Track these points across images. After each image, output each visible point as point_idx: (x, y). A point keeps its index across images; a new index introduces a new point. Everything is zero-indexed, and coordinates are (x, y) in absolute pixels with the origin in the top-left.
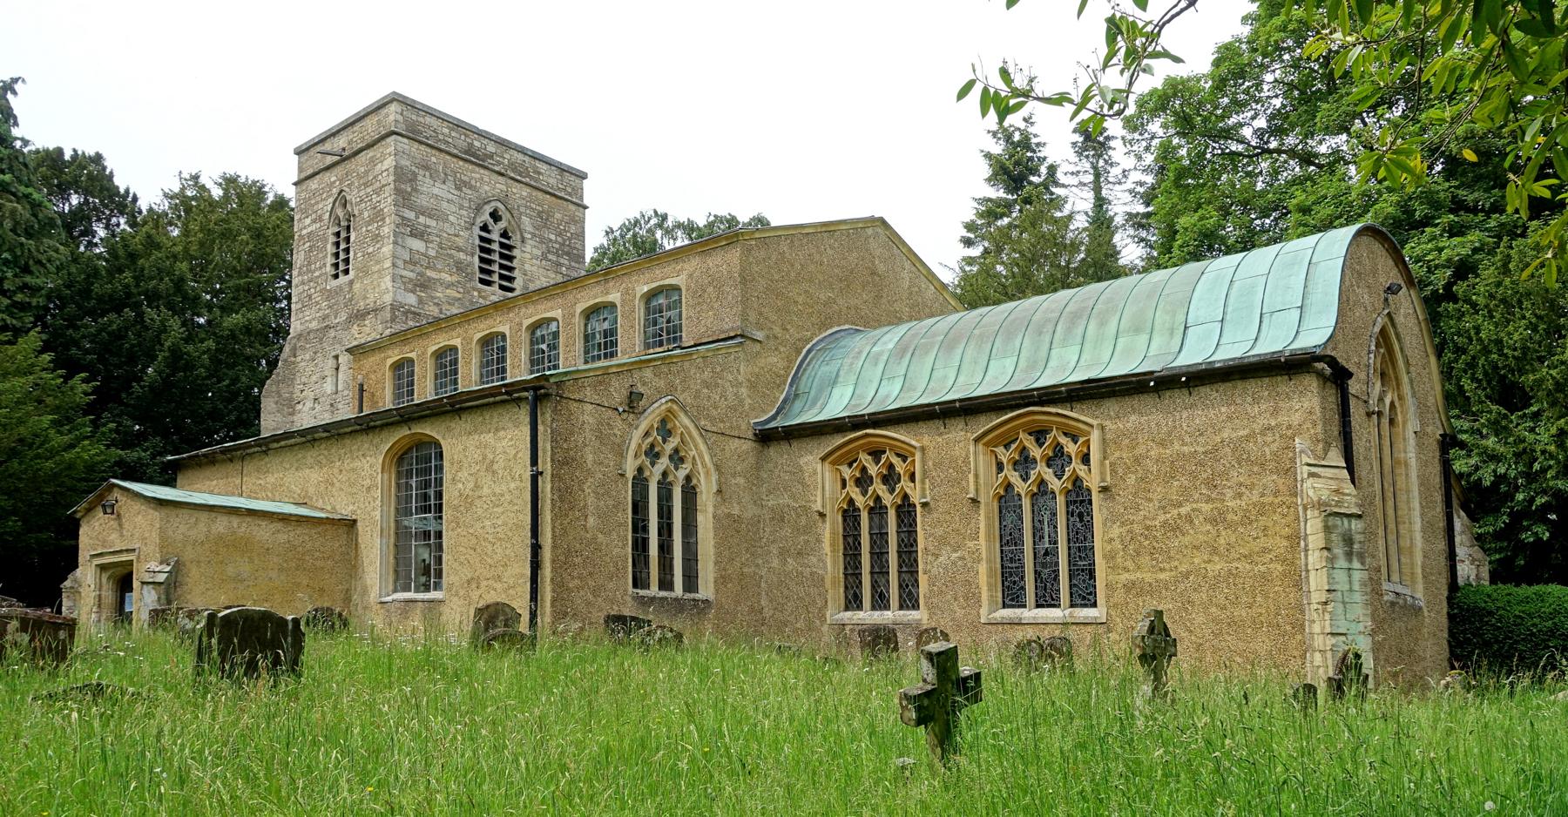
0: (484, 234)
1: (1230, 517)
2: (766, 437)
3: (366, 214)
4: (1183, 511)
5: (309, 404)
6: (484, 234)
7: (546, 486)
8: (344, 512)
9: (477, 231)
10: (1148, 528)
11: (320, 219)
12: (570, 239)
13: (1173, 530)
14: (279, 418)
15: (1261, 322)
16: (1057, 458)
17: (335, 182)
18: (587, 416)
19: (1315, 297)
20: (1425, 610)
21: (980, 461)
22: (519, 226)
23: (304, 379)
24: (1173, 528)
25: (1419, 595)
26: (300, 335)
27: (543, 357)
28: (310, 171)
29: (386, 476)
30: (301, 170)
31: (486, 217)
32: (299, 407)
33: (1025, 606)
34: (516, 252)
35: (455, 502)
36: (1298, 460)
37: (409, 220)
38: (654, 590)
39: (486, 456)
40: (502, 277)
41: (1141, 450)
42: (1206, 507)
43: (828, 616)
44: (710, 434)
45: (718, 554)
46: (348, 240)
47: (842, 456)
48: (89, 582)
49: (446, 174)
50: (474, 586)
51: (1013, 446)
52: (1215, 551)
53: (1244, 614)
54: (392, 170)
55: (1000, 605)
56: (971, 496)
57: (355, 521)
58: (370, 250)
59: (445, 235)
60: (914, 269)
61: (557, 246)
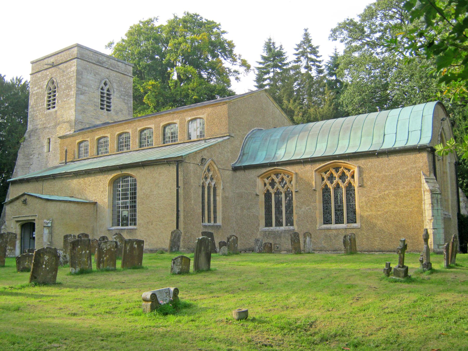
0: (102, 91)
1: (401, 194)
2: (235, 169)
3: (63, 87)
4: (386, 193)
5: (36, 156)
6: (102, 91)
7: (181, 191)
8: (91, 199)
9: (100, 90)
10: (374, 198)
11: (42, 88)
12: (128, 90)
13: (383, 199)
14: (24, 161)
15: (408, 134)
16: (343, 176)
17: (49, 74)
18: (192, 167)
19: (425, 128)
20: (452, 219)
21: (260, 183)
22: (113, 87)
23: (33, 147)
24: (383, 198)
25: (450, 214)
26: (32, 130)
27: (145, 141)
28: (37, 70)
29: (110, 187)
30: (33, 69)
31: (103, 85)
32: (31, 157)
33: (332, 224)
34: (112, 96)
35: (142, 196)
36: (422, 177)
37: (80, 89)
38: (206, 223)
39: (155, 181)
40: (107, 106)
41: (372, 174)
42: (393, 191)
43: (260, 229)
44: (221, 170)
45: (223, 210)
46: (55, 96)
47: (265, 175)
48: (12, 226)
49: (91, 71)
50: (150, 224)
51: (328, 173)
52: (396, 205)
53: (405, 224)
54: (75, 71)
55: (323, 224)
56: (314, 189)
57: (96, 203)
58: (65, 100)
59: (90, 93)
60: (273, 105)
61: (124, 93)
